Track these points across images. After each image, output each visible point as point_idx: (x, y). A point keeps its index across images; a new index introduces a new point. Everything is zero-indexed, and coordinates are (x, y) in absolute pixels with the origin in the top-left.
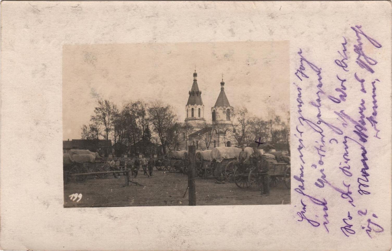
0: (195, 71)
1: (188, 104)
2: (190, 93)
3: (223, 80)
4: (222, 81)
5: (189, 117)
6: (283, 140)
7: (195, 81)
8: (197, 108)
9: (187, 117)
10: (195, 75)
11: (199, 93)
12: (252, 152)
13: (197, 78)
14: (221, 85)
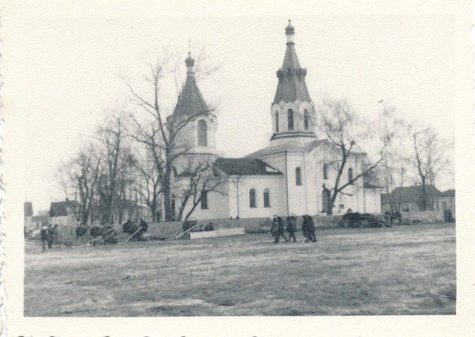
1: (277, 101)
2: (280, 74)
3: (291, 23)
4: (290, 24)
5: (281, 131)
6: (425, 166)
7: (290, 44)
9: (277, 130)
10: (290, 31)
12: (269, 166)
13: (295, 39)
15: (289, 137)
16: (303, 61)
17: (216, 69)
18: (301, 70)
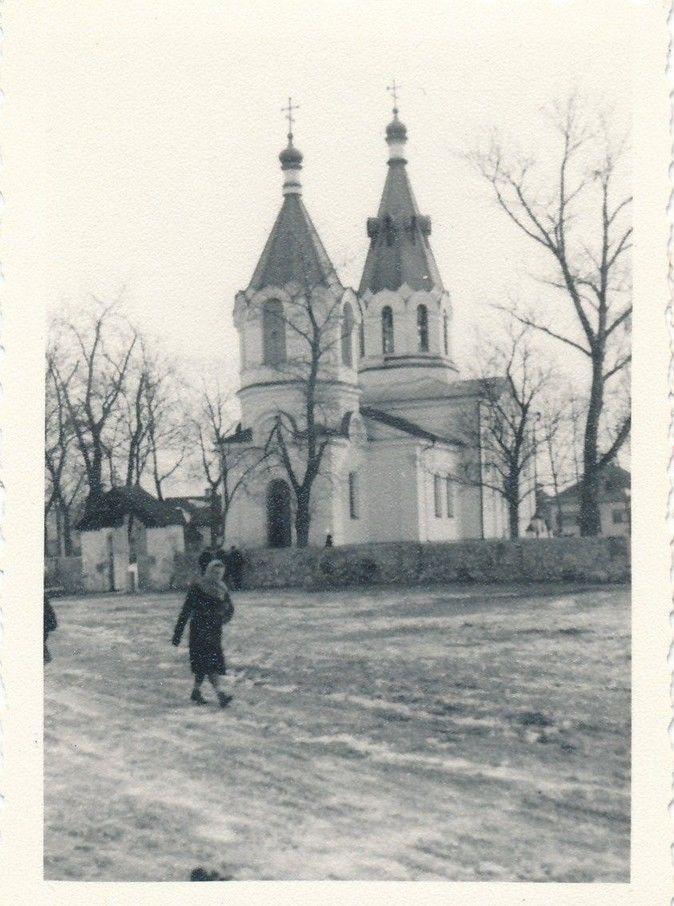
0: (297, 107)
4: (290, 144)
7: (397, 164)
8: (413, 306)
10: (396, 133)
11: (419, 227)
13: (407, 151)
14: (283, 168)
15: (424, 366)
16: (425, 203)
17: (499, 196)
18: (414, 219)
